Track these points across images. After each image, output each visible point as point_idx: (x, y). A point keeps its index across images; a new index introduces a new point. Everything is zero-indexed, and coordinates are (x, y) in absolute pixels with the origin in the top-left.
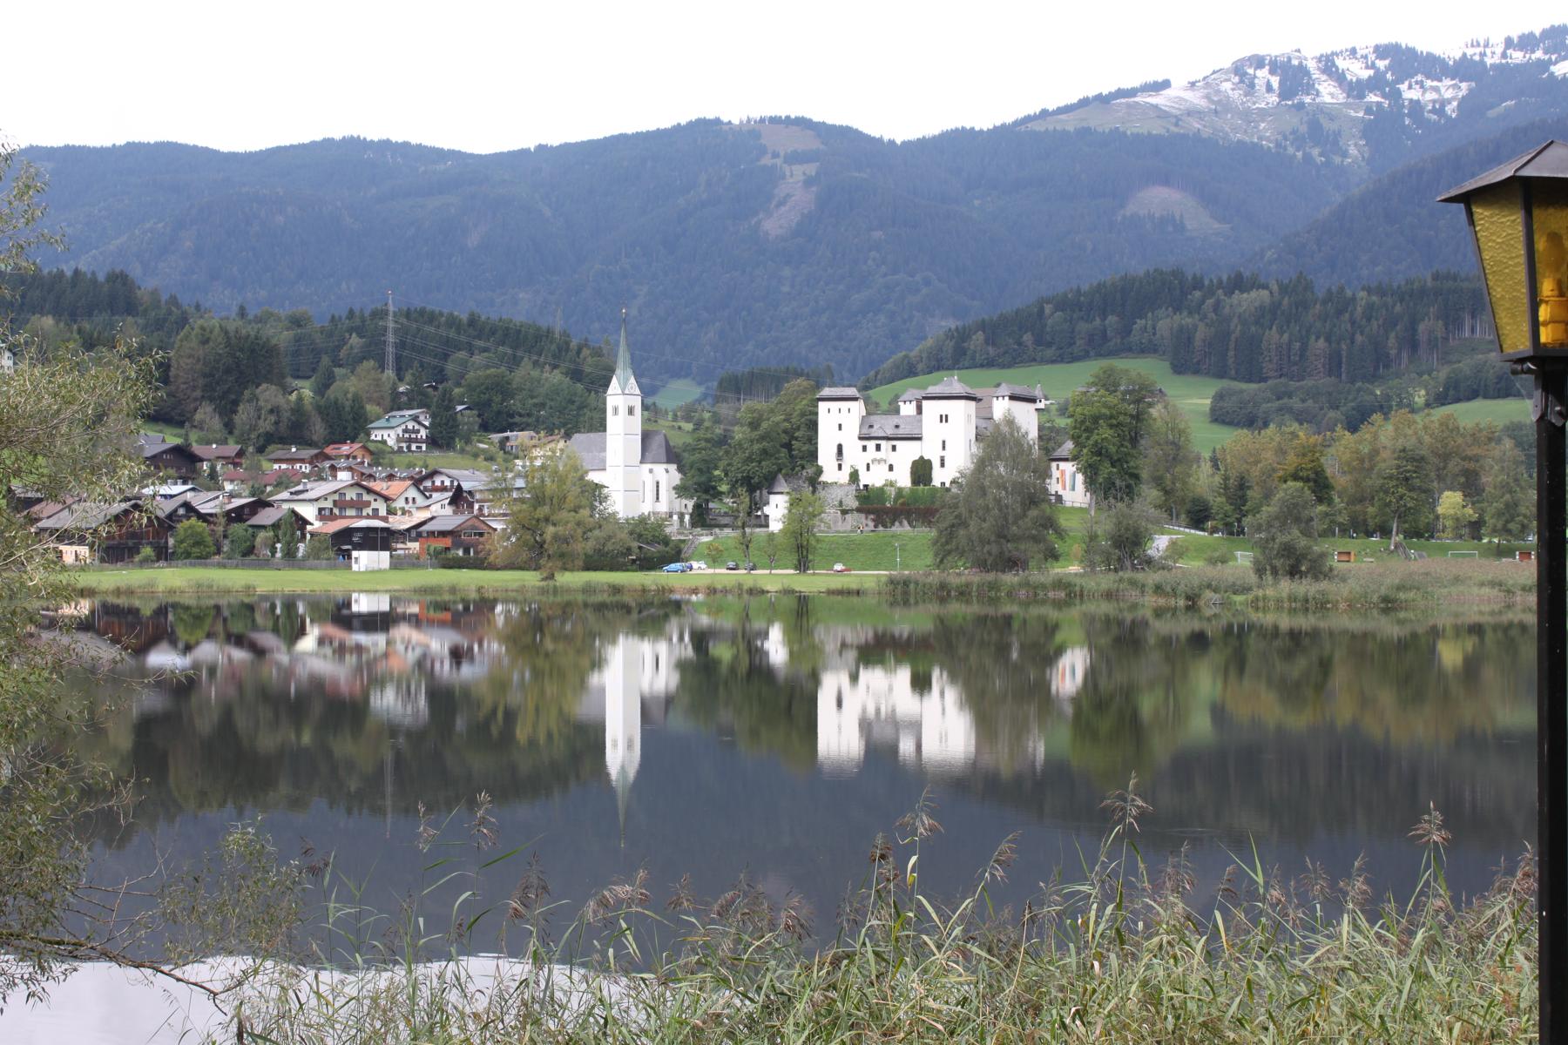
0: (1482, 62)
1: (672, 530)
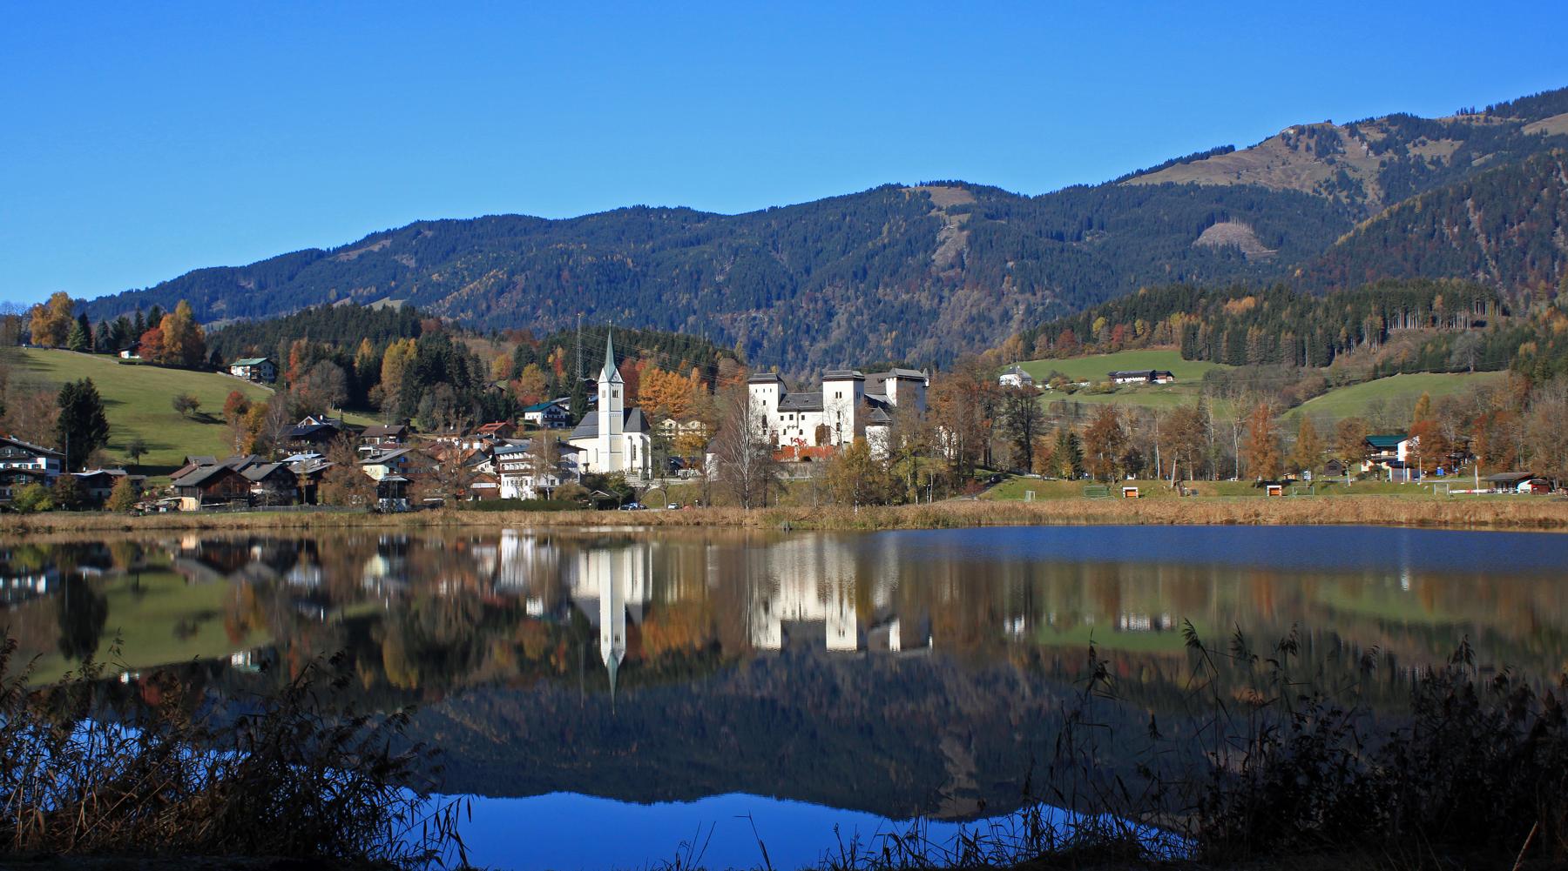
1: (635, 482)
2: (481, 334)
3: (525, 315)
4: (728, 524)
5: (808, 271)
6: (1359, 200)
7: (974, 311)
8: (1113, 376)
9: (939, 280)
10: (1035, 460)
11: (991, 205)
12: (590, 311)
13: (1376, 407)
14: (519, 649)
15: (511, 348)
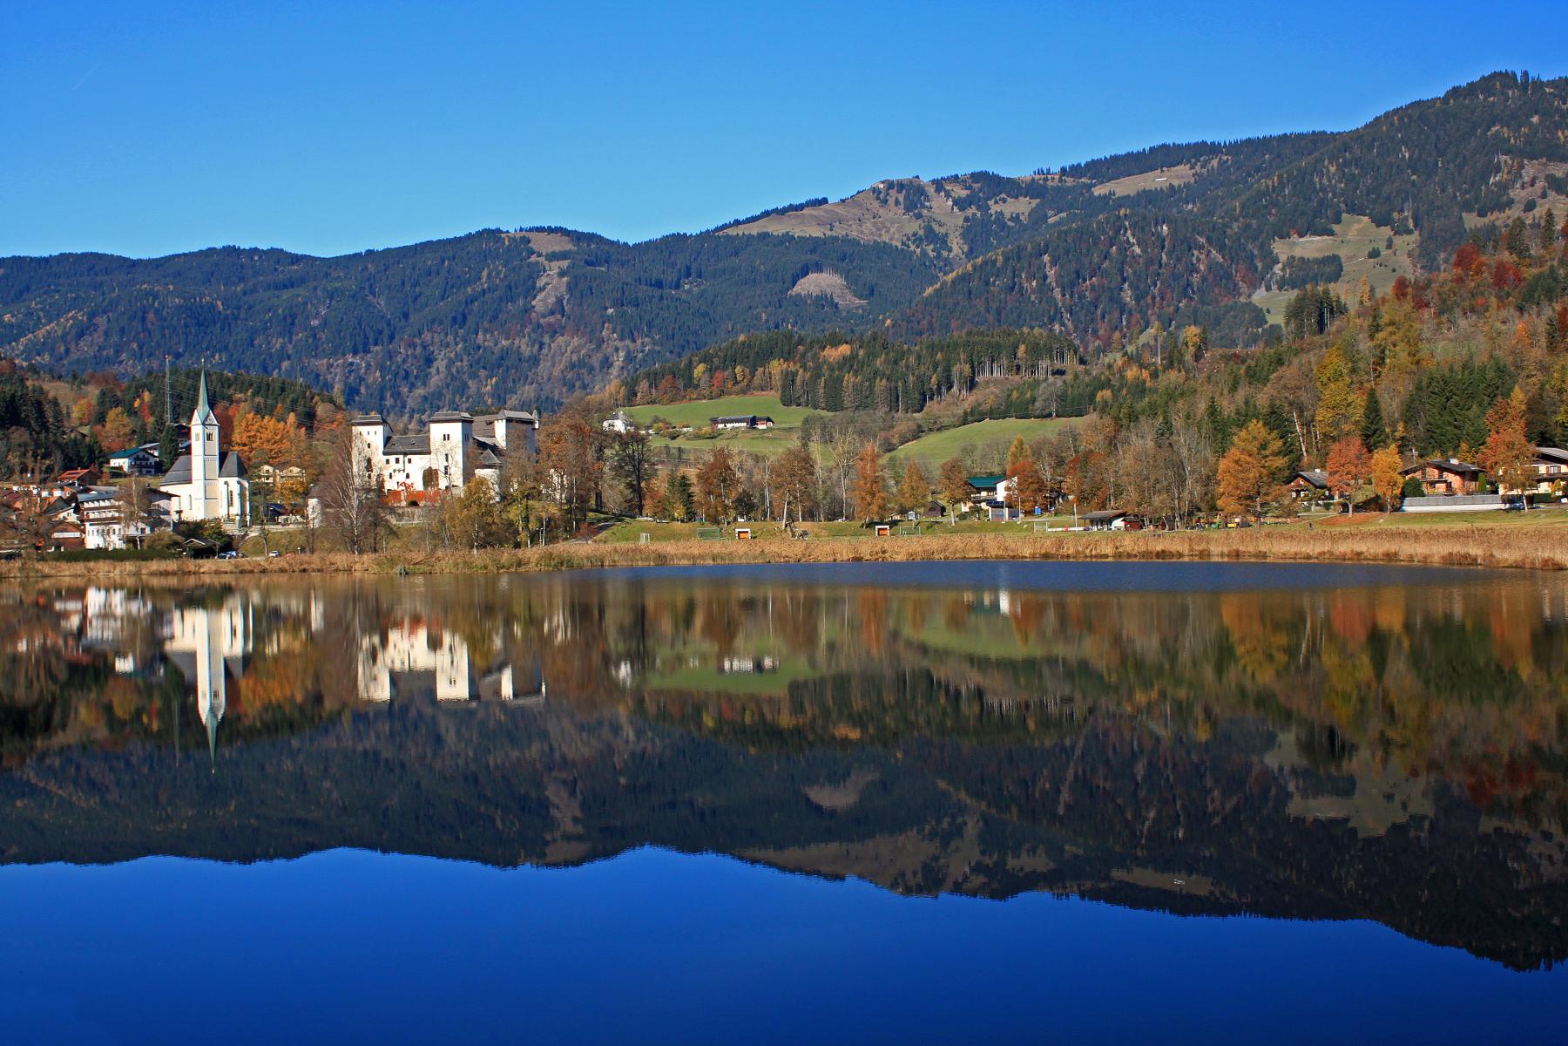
0: (1045, 186)
1: (232, 529)
2: (60, 377)
3: (108, 361)
4: (337, 570)
5: (406, 316)
6: (945, 253)
7: (575, 358)
8: (715, 421)
9: (539, 326)
10: (648, 504)
11: (591, 252)
12: (178, 356)
13: (968, 451)
14: (109, 709)
15: (93, 392)
